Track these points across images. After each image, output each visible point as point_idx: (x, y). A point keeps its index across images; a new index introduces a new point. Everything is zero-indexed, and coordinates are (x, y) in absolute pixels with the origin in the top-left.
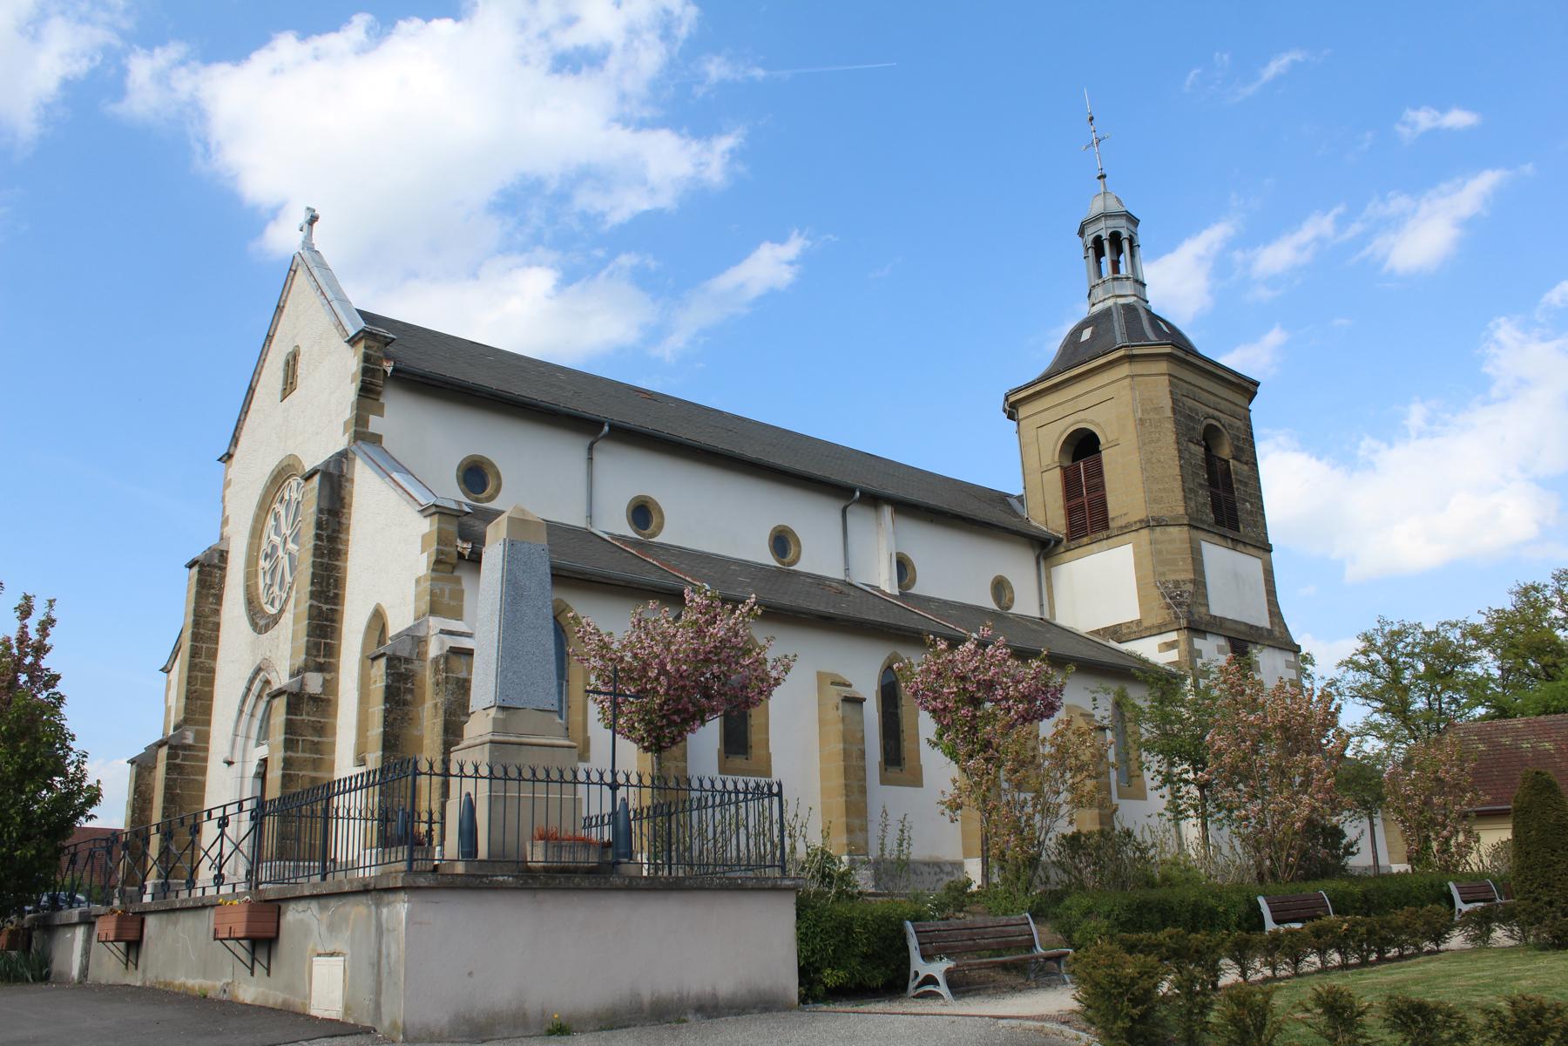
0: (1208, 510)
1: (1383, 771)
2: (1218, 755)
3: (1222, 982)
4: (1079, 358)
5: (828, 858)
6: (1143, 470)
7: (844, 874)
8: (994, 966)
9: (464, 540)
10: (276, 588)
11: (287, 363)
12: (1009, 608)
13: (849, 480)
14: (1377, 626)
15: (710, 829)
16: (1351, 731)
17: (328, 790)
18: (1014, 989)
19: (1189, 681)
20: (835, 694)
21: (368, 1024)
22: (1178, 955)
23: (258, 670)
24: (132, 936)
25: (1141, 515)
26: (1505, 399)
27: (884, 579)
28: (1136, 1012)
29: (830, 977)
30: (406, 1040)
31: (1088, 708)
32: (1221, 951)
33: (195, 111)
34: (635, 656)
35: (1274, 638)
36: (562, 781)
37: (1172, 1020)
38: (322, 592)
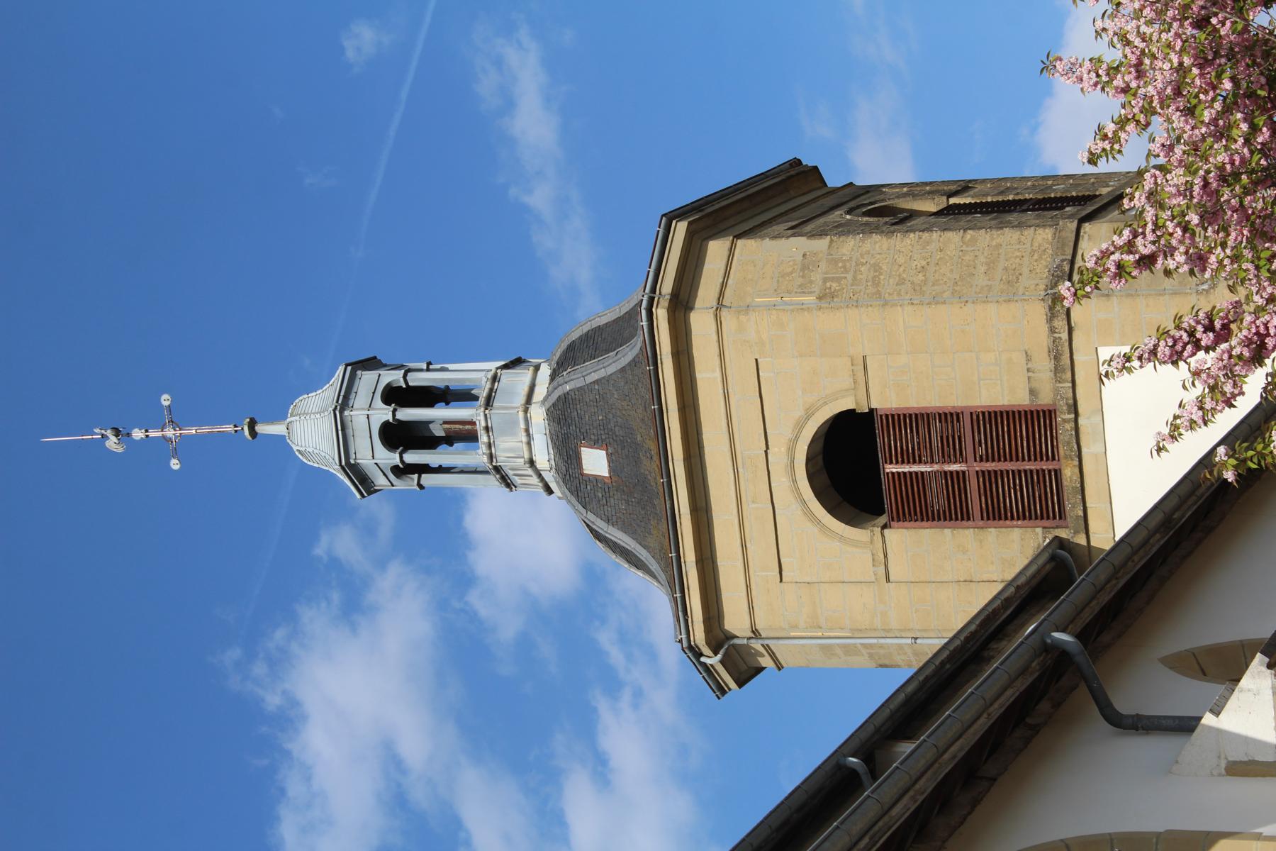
6: (936, 300)
25: (1039, 311)
26: (944, 303)
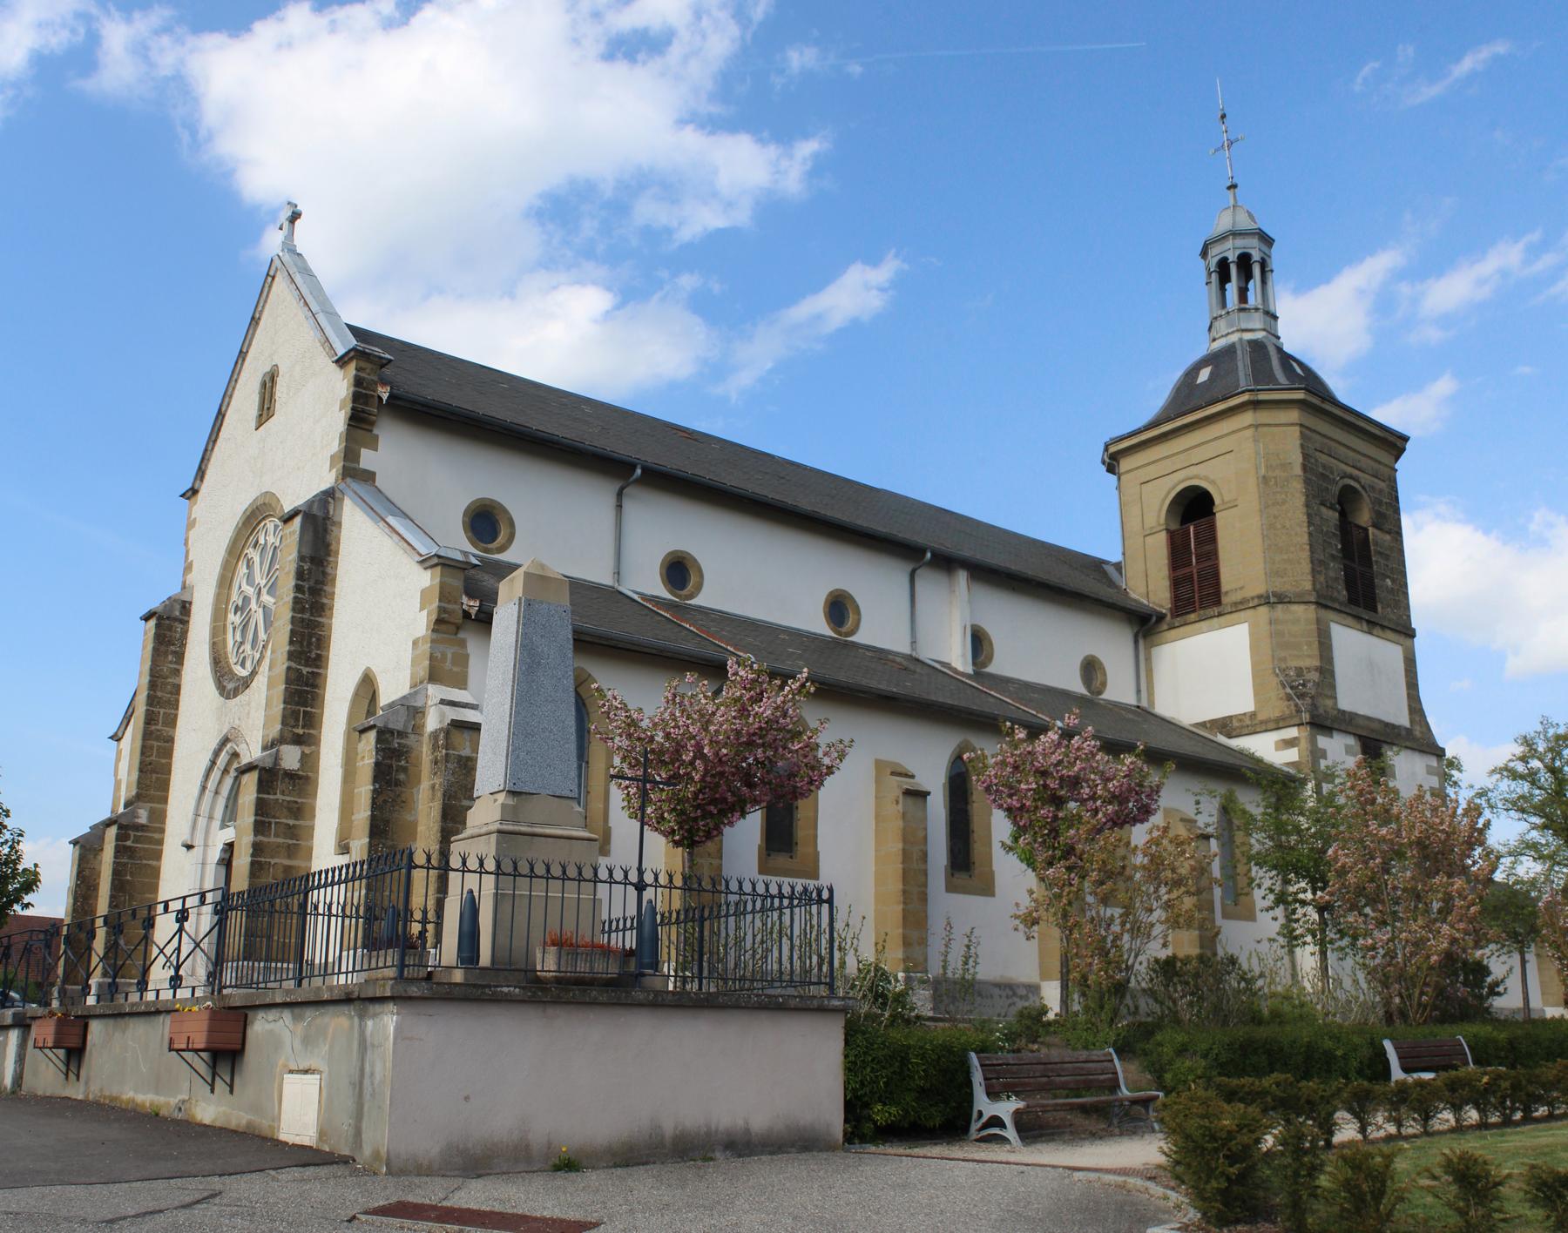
0: (1341, 587)
1: (1538, 899)
2: (1342, 872)
3: (1338, 1138)
4: (1193, 404)
5: (883, 976)
7: (903, 994)
8: (1072, 1108)
9: (471, 596)
10: (247, 647)
11: (264, 385)
12: (1100, 693)
13: (919, 539)
14: (1540, 728)
15: (749, 938)
16: (1503, 850)
17: (304, 883)
18: (1095, 1136)
19: (1310, 786)
20: (895, 785)
21: (346, 1152)
22: (1288, 1105)
23: (225, 741)
24: (74, 1042)
25: (1260, 589)
27: (957, 657)
28: (1233, 1170)
29: (881, 1113)
30: (390, 1173)
31: (1190, 812)
32: (1336, 1102)
33: (180, 87)
34: (667, 736)
35: (1415, 739)
36: (580, 879)
37: (1276, 1182)
38: (301, 653)
